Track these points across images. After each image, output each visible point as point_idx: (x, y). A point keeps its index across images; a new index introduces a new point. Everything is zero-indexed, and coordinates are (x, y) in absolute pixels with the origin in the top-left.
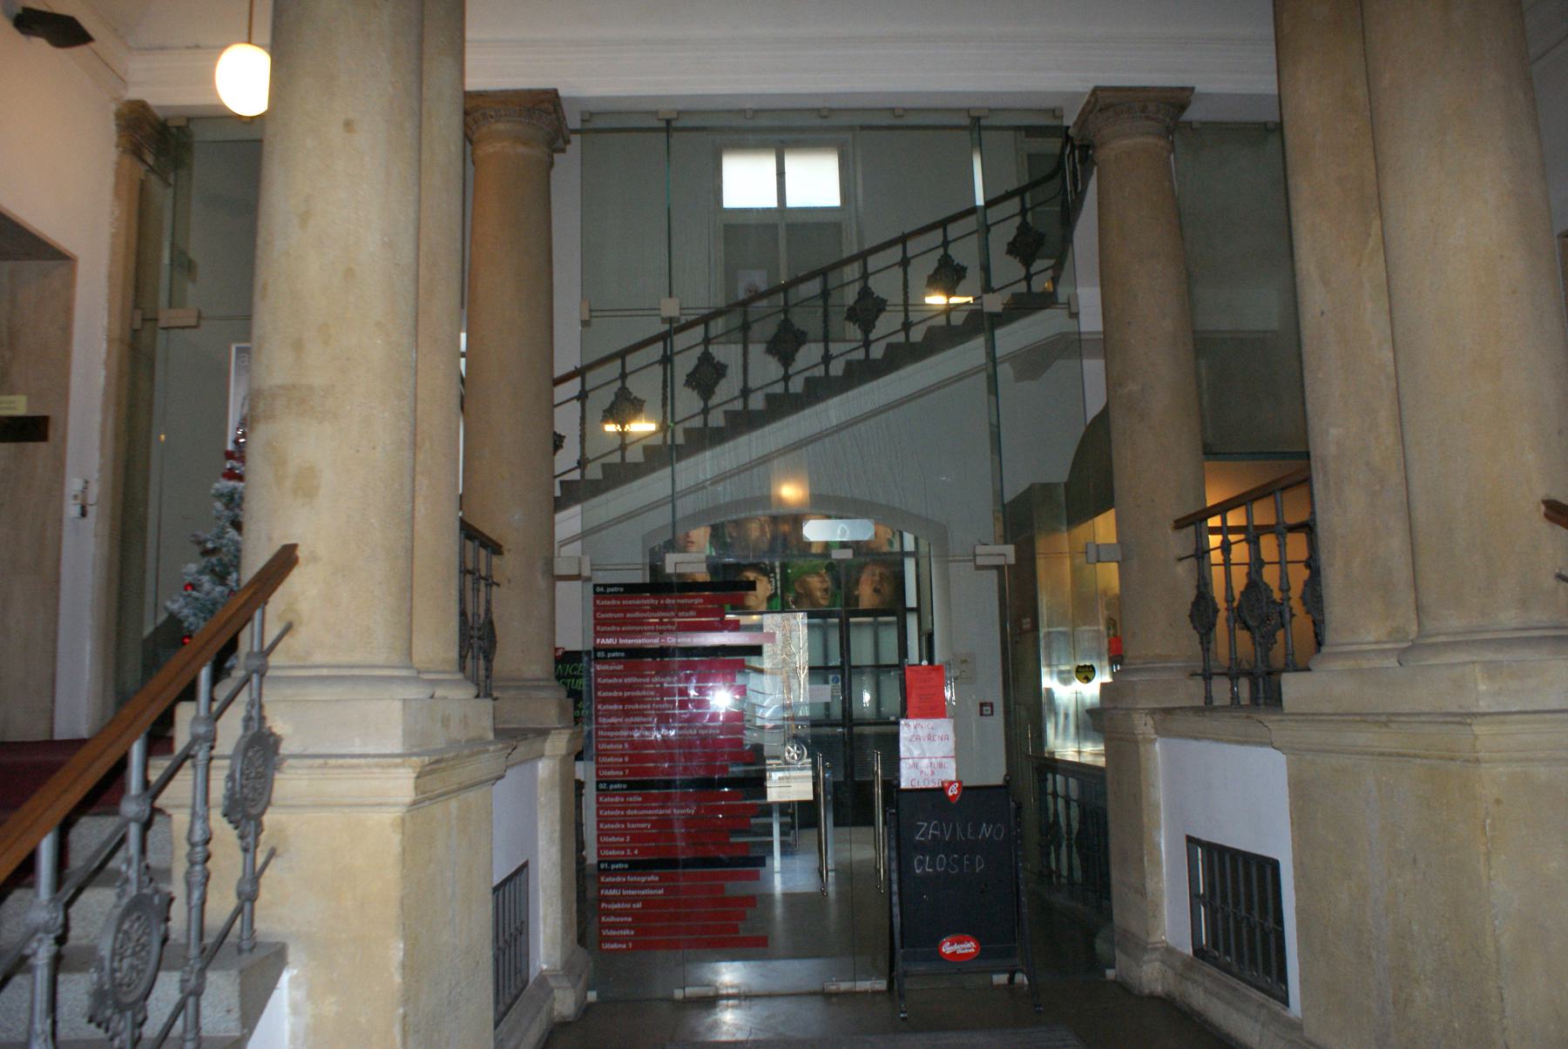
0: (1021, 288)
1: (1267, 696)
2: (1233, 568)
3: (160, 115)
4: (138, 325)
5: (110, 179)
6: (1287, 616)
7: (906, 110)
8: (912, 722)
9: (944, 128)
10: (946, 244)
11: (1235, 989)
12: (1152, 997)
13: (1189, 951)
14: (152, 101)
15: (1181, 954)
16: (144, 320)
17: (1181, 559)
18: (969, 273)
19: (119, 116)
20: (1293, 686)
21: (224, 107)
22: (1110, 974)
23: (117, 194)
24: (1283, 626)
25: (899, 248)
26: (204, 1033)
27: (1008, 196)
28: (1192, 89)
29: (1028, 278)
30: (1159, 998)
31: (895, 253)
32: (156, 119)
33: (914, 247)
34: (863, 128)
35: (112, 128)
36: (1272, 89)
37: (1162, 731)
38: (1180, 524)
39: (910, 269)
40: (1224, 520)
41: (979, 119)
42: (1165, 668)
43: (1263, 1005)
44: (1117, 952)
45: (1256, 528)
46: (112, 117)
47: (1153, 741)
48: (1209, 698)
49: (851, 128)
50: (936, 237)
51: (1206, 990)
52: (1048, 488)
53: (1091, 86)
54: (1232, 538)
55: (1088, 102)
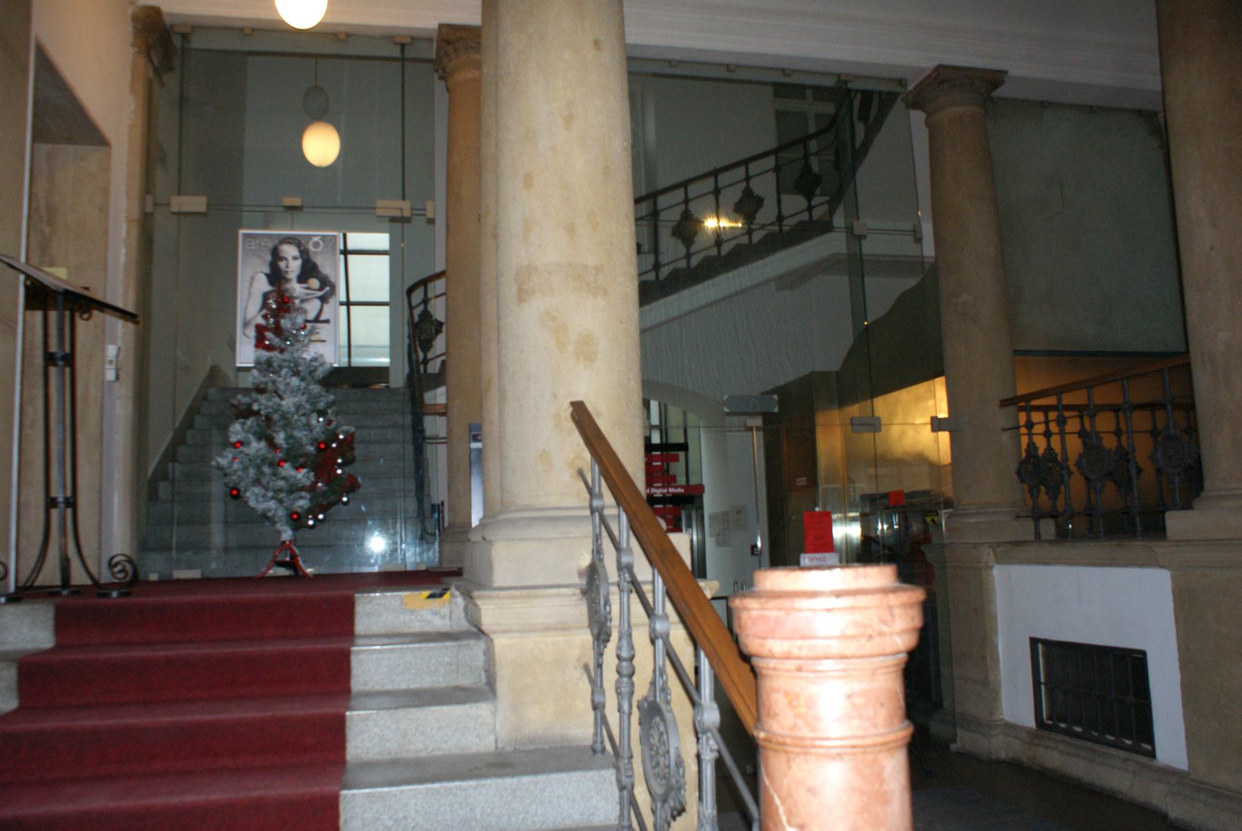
0: (805, 217)
1: (1156, 529)
2: (1067, 437)
3: (168, 21)
4: (149, 208)
5: (127, 78)
6: (1134, 473)
7: (794, 71)
8: (807, 555)
9: (706, 79)
10: (748, 178)
11: (1093, 750)
12: (1000, 762)
13: (1031, 723)
14: (165, 9)
15: (1022, 728)
16: (155, 204)
17: (1005, 430)
18: (765, 203)
19: (135, 18)
20: (1176, 521)
21: (283, 22)
22: (953, 747)
23: (133, 90)
24: (1063, 482)
25: (712, 180)
26: (610, 774)
27: (794, 143)
28: (1006, 72)
29: (810, 209)
30: (1004, 762)
31: (709, 184)
32: (164, 25)
33: (724, 179)
34: (655, 75)
35: (129, 28)
36: (1158, 87)
37: (999, 561)
38: (1004, 403)
39: (721, 197)
40: (1059, 400)
41: (846, 82)
42: (995, 513)
43: (1128, 760)
44: (959, 730)
45: (1096, 406)
46: (130, 20)
47: (991, 568)
48: (1038, 536)
49: (646, 74)
50: (740, 173)
51: (1062, 752)
52: (825, 375)
53: (935, 64)
54: (1067, 414)
55: (929, 76)
